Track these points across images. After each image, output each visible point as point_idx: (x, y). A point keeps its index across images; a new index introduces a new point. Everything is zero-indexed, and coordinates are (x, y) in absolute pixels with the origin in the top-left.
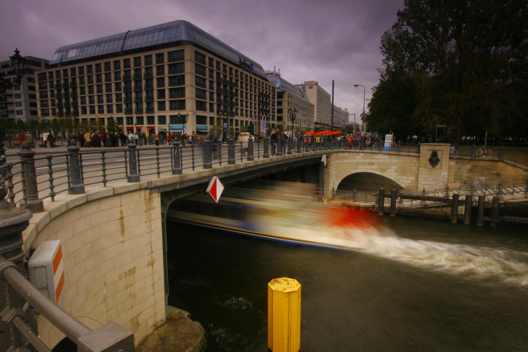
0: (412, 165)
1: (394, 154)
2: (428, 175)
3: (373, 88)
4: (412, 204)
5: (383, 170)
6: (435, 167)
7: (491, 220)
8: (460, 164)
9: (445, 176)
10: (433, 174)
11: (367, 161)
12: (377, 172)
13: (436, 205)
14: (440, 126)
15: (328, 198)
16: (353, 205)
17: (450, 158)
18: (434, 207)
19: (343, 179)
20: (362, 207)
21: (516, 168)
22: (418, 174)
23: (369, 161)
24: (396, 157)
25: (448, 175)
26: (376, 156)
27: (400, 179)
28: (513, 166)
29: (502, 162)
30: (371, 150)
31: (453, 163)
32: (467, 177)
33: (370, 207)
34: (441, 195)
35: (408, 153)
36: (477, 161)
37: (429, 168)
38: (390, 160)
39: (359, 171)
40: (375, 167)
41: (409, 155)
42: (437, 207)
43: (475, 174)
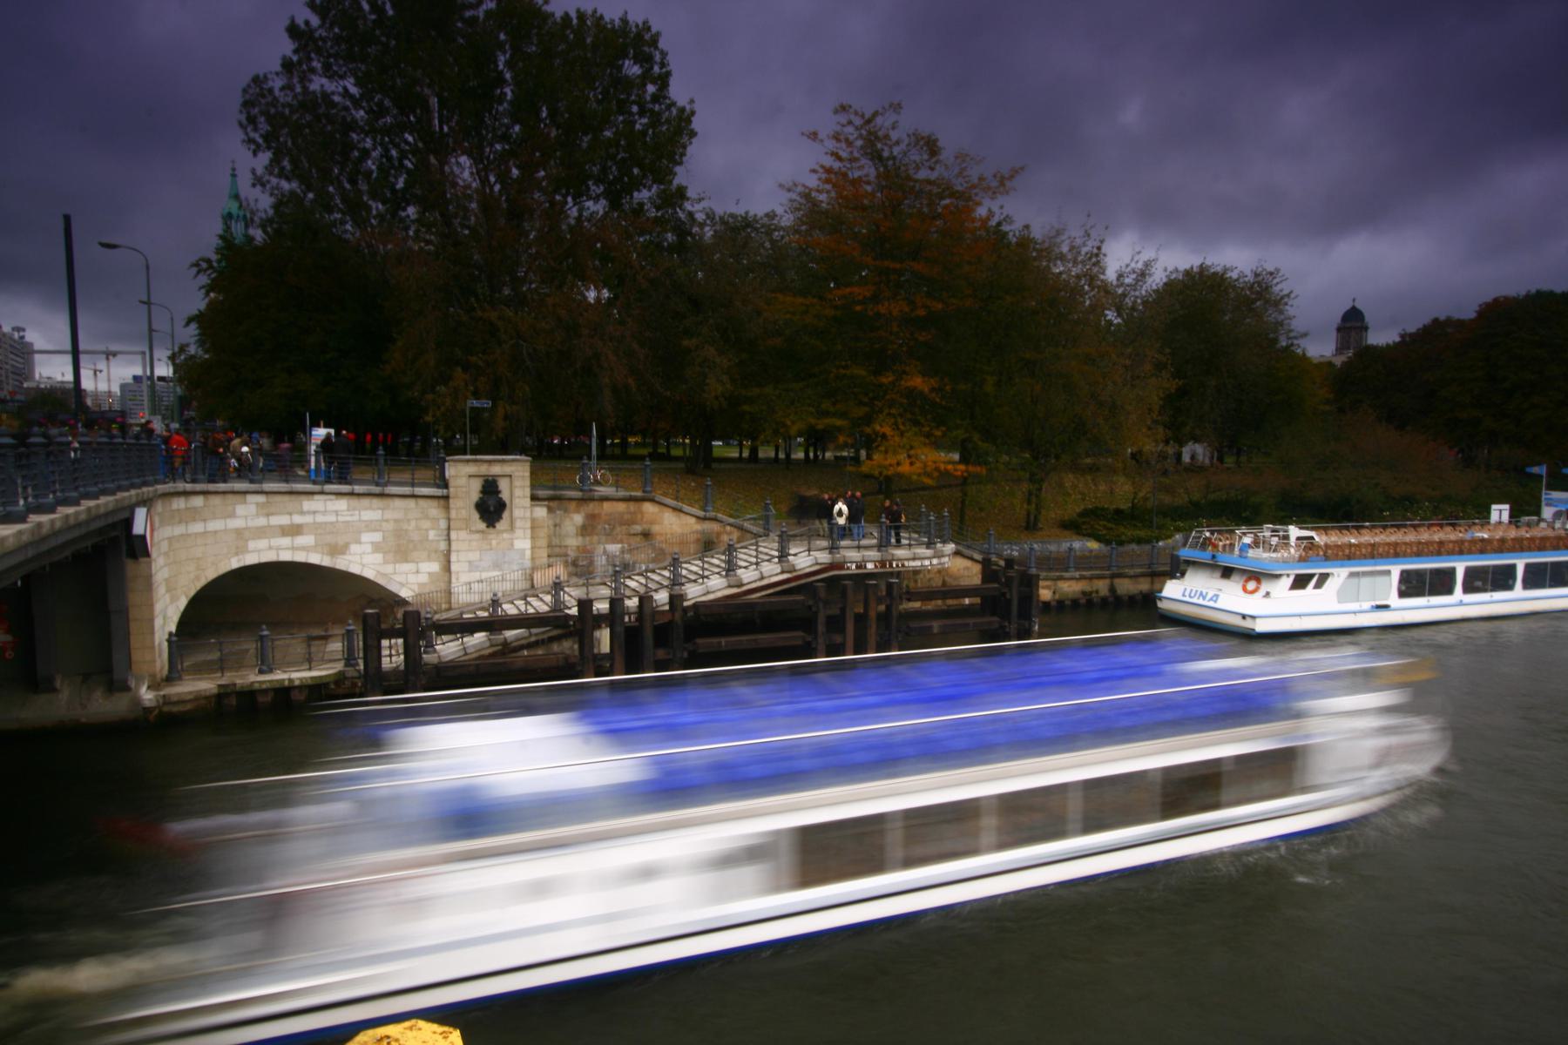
0: (426, 524)
1: (366, 492)
2: (478, 553)
3: (196, 265)
4: (464, 648)
5: (336, 550)
6: (494, 527)
7: (671, 657)
8: (558, 512)
9: (524, 550)
10: (491, 549)
11: (277, 520)
12: (315, 559)
13: (533, 639)
14: (476, 403)
15: (153, 676)
16: (264, 686)
17: (534, 498)
18: (529, 646)
19: (192, 593)
20: (301, 687)
21: (682, 515)
22: (449, 551)
23: (284, 520)
24: (376, 502)
25: (533, 548)
26: (309, 504)
27: (395, 573)
28: (675, 509)
29: (652, 500)
30: (287, 481)
31: (541, 512)
32: (578, 547)
33: (328, 680)
34: (541, 605)
35: (411, 489)
36: (596, 503)
37: (478, 532)
38: (357, 512)
39: (251, 559)
40: (306, 540)
41: (416, 493)
42: (536, 644)
43: (595, 538)
